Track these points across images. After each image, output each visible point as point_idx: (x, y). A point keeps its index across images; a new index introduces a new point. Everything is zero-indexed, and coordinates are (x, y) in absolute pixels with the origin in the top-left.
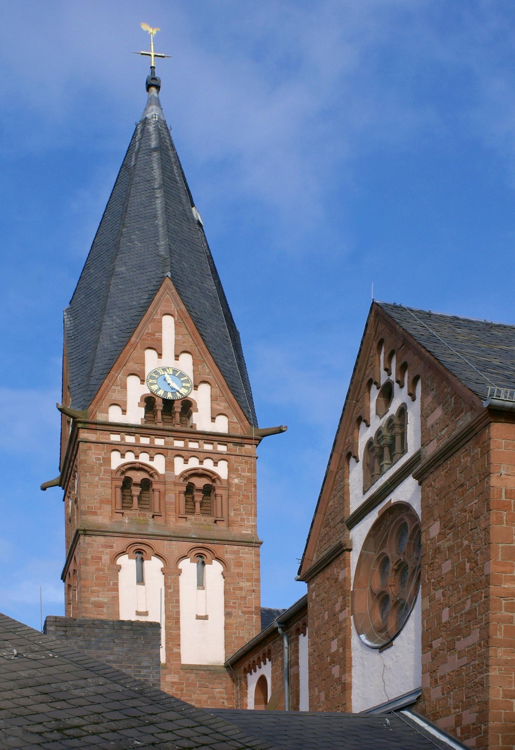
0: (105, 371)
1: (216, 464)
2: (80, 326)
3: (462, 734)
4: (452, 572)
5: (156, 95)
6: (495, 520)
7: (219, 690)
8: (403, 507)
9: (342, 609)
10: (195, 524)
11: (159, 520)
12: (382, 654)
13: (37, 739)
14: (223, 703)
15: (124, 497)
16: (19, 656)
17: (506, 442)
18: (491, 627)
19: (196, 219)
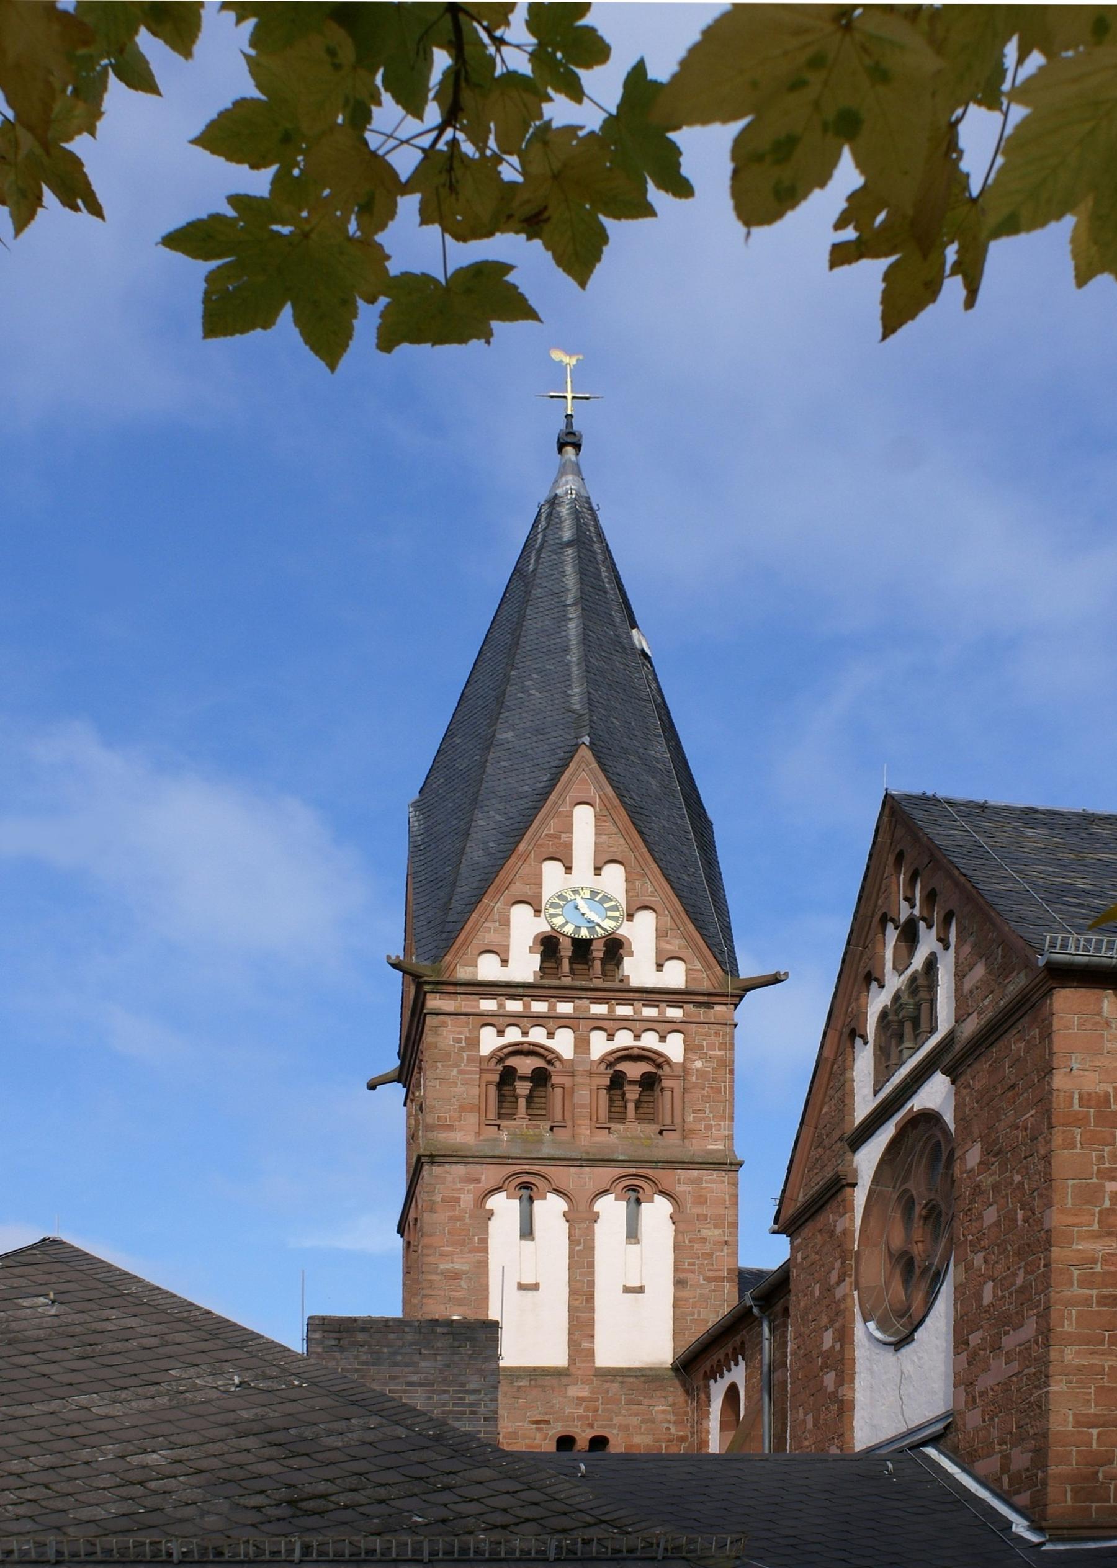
0: (473, 900)
1: (663, 1039)
2: (435, 829)
3: (1010, 1486)
4: (997, 1224)
5: (573, 458)
6: (1060, 1142)
7: (661, 1408)
8: (930, 1117)
9: (841, 1281)
10: (628, 1136)
11: (562, 1134)
12: (899, 1355)
13: (255, 1517)
14: (668, 1429)
15: (501, 1098)
16: (244, 1385)
17: (1079, 1019)
18: (1054, 1315)
19: (639, 647)
